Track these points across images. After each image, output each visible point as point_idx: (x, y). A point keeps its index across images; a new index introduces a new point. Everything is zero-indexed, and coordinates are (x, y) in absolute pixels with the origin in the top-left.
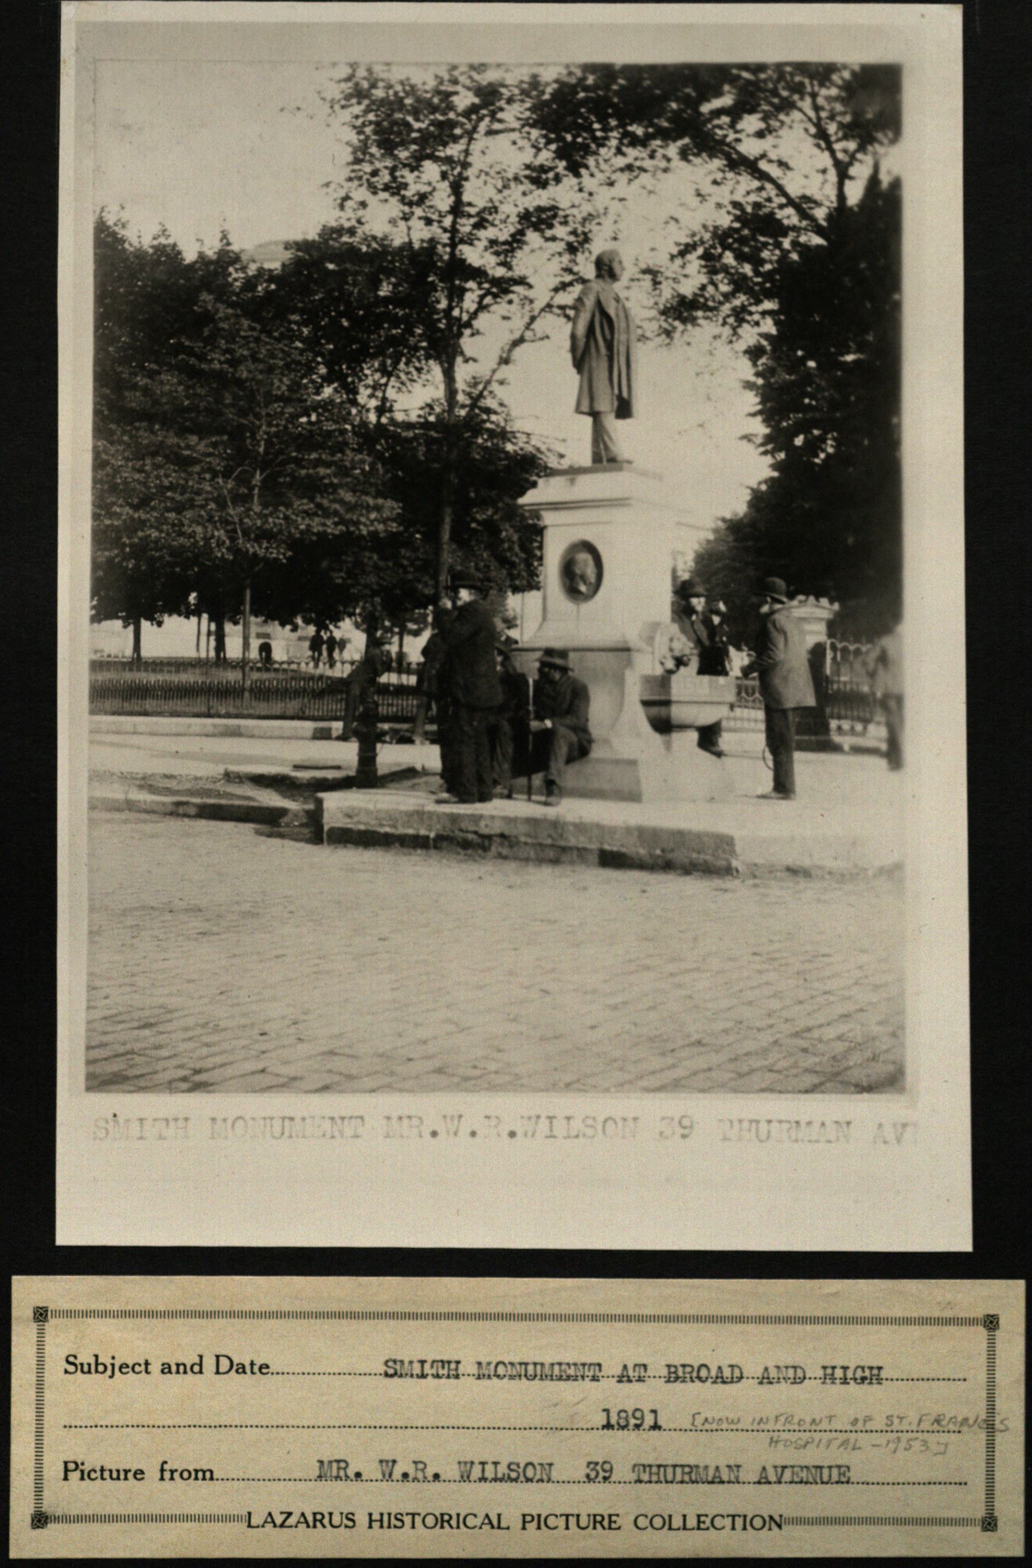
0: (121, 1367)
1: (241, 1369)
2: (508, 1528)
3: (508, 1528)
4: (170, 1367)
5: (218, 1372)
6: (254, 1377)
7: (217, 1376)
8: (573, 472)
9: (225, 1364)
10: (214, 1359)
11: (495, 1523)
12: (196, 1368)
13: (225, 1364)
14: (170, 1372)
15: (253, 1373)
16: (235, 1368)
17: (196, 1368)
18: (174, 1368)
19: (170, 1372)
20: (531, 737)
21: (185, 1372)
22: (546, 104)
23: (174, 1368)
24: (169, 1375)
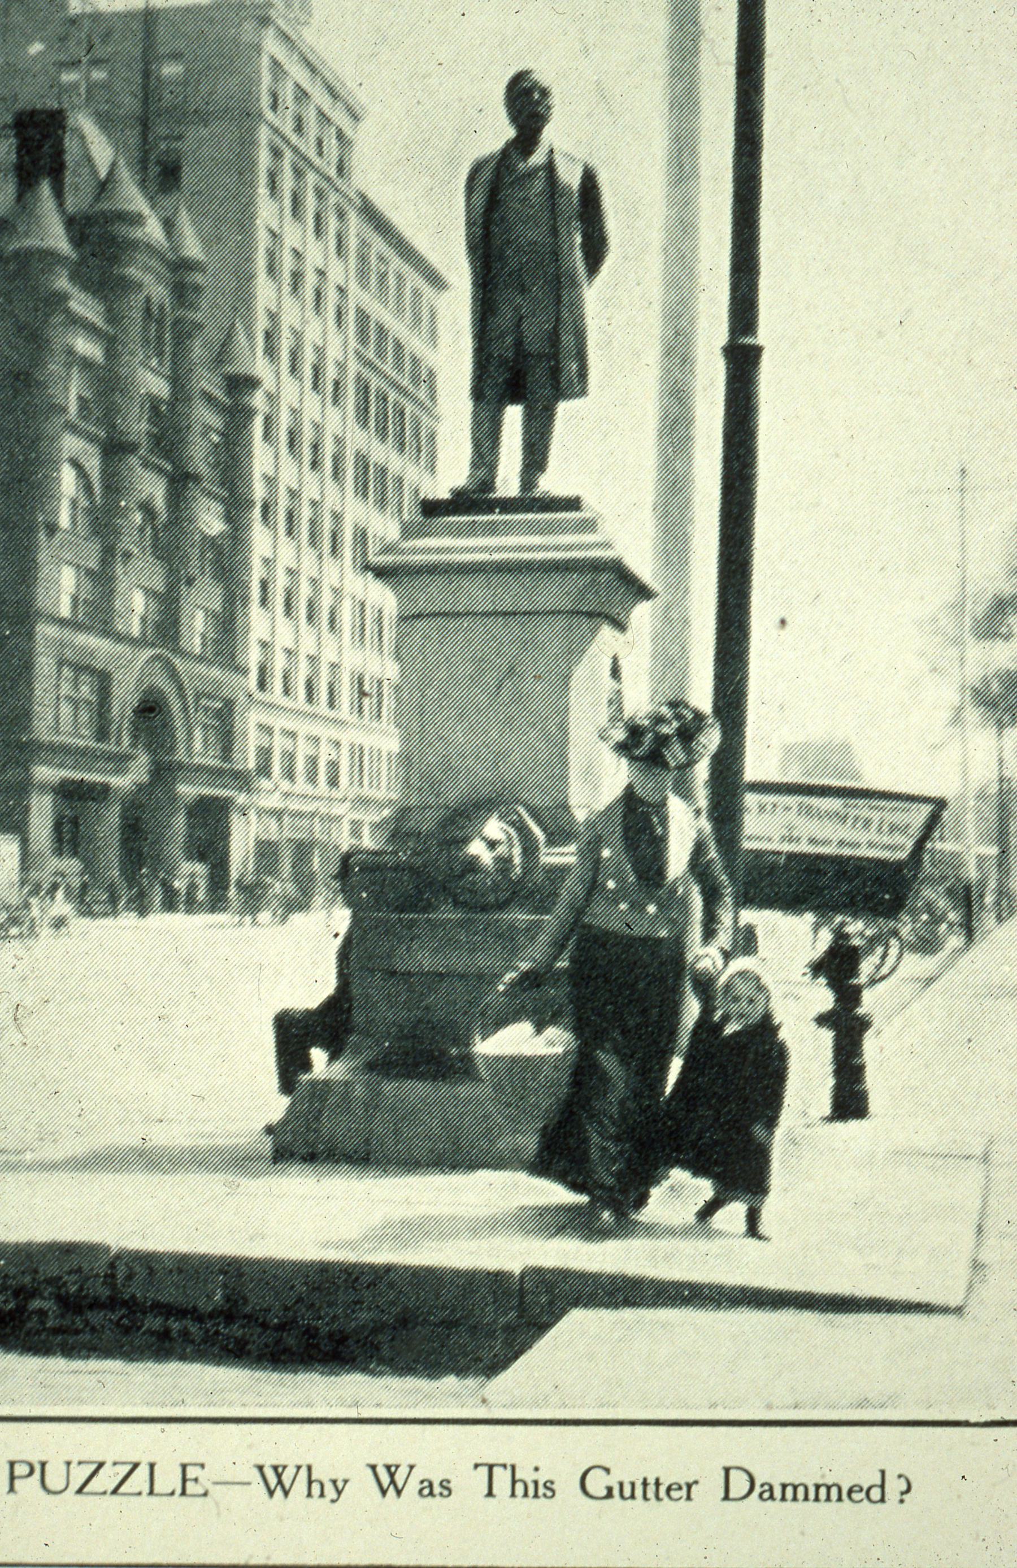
0: (669, 1489)
1: (768, 1493)
2: (476, 1466)
3: (476, 1466)
4: (771, 1489)
5: (726, 1497)
6: (647, 1503)
7: (726, 1503)
8: (120, 638)
9: (739, 1484)
10: (495, 1491)
11: (857, 845)
12: (875, 1495)
13: (739, 1484)
14: (772, 1497)
15: (658, 1498)
16: (758, 1490)
17: (875, 1495)
18: (778, 1493)
19: (772, 1497)
20: (180, 822)
21: (840, 1499)
22: (82, 261)
23: (778, 1493)
24: (769, 1502)
